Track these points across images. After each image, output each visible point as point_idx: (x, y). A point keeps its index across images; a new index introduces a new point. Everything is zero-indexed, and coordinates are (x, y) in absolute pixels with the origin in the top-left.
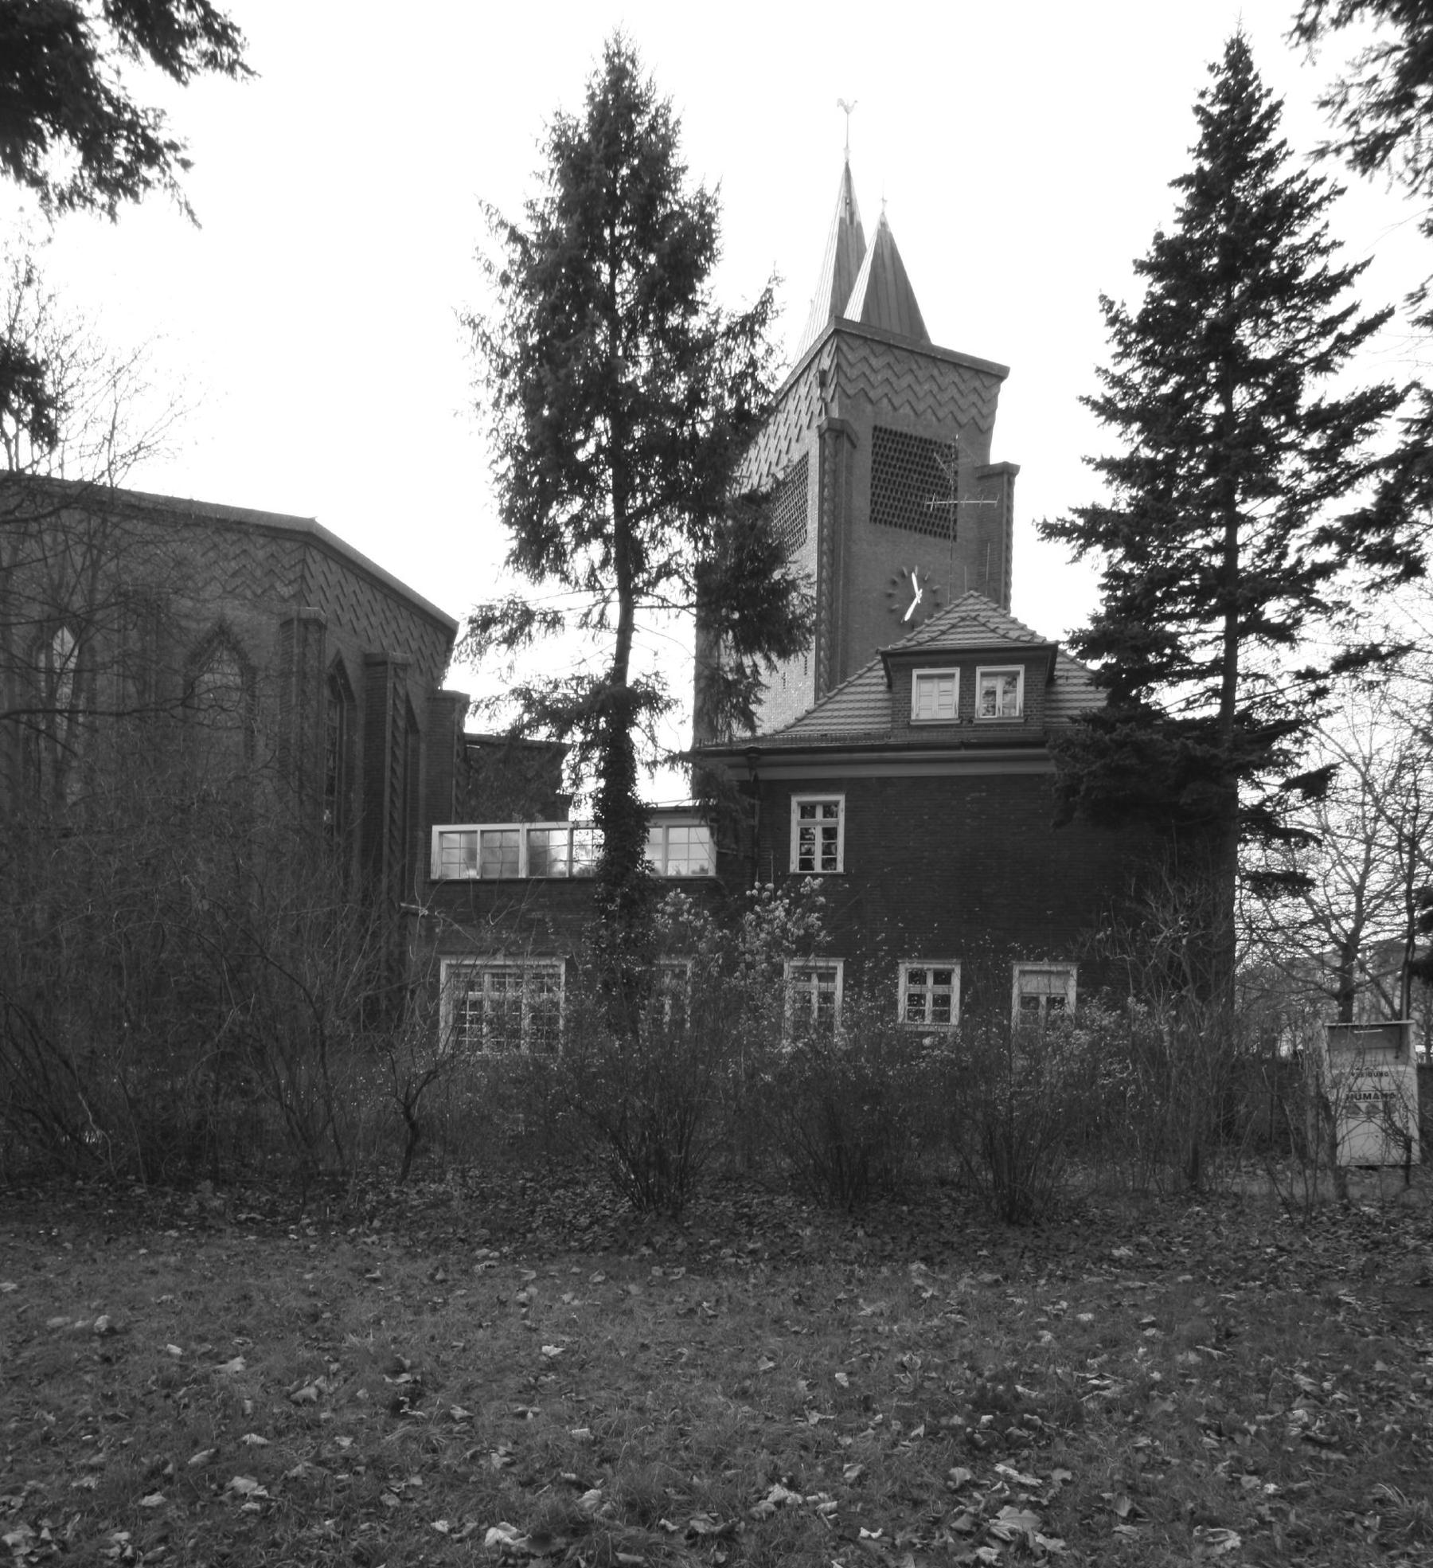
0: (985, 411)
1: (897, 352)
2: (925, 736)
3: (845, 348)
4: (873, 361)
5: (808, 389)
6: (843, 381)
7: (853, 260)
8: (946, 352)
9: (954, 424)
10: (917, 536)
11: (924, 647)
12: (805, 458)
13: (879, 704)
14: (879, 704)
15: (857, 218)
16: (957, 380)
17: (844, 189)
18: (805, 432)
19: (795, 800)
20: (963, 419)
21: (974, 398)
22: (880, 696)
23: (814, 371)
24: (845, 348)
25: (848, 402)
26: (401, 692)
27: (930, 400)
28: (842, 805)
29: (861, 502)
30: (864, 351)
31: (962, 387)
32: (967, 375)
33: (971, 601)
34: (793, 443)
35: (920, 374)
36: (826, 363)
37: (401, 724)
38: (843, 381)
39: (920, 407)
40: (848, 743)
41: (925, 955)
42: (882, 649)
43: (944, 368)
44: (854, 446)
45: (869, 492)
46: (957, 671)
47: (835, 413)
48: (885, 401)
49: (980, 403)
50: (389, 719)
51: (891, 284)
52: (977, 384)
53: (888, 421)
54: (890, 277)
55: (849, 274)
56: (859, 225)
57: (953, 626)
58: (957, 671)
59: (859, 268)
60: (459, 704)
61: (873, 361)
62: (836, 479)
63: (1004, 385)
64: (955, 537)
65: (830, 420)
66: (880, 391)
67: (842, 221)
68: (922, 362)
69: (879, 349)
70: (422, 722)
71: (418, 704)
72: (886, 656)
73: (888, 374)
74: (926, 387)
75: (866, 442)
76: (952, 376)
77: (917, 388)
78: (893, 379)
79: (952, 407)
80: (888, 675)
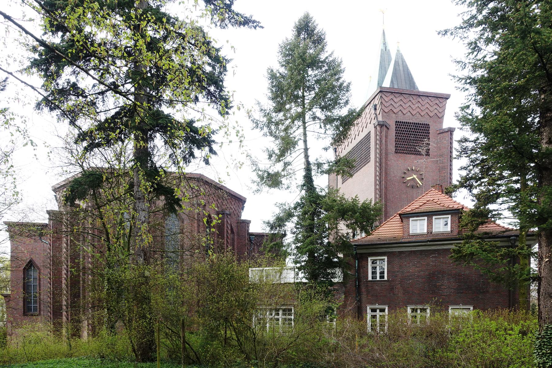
0: (440, 115)
1: (404, 95)
2: (413, 239)
3: (384, 97)
4: (395, 100)
5: (369, 110)
6: (383, 108)
7: (386, 63)
8: (424, 92)
9: (428, 116)
10: (414, 156)
11: (414, 211)
12: (368, 135)
13: (398, 227)
14: (398, 227)
15: (388, 48)
16: (429, 101)
17: (382, 39)
18: (369, 124)
19: (369, 259)
20: (431, 114)
21: (436, 107)
22: (399, 225)
23: (372, 105)
24: (384, 97)
25: (385, 114)
26: (229, 222)
27: (418, 110)
28: (386, 260)
29: (392, 147)
30: (392, 97)
31: (431, 103)
32: (433, 99)
33: (432, 192)
34: (364, 128)
35: (413, 101)
36: (376, 101)
37: (229, 232)
38: (383, 108)
39: (414, 113)
40: (388, 242)
41: (416, 304)
42: (399, 212)
43: (423, 98)
44: (388, 129)
45: (394, 143)
46: (426, 218)
47: (380, 118)
48: (400, 112)
49: (438, 108)
50: (225, 230)
51: (402, 72)
52: (437, 102)
53: (401, 119)
54: (401, 68)
55: (385, 68)
56: (389, 50)
57: (425, 204)
58: (426, 218)
59: (389, 65)
60: (247, 223)
61: (395, 100)
62: (381, 141)
63: (448, 101)
64: (428, 154)
65: (379, 122)
66: (398, 109)
67: (382, 50)
68: (414, 97)
69: (397, 95)
70: (235, 230)
71: (234, 225)
72: (400, 215)
73: (401, 103)
74: (417, 105)
75: (393, 127)
76: (427, 100)
77: (412, 106)
78: (403, 105)
79: (427, 111)
80: (401, 218)
